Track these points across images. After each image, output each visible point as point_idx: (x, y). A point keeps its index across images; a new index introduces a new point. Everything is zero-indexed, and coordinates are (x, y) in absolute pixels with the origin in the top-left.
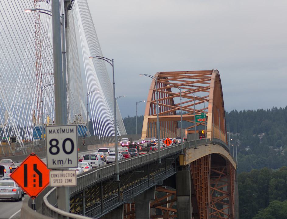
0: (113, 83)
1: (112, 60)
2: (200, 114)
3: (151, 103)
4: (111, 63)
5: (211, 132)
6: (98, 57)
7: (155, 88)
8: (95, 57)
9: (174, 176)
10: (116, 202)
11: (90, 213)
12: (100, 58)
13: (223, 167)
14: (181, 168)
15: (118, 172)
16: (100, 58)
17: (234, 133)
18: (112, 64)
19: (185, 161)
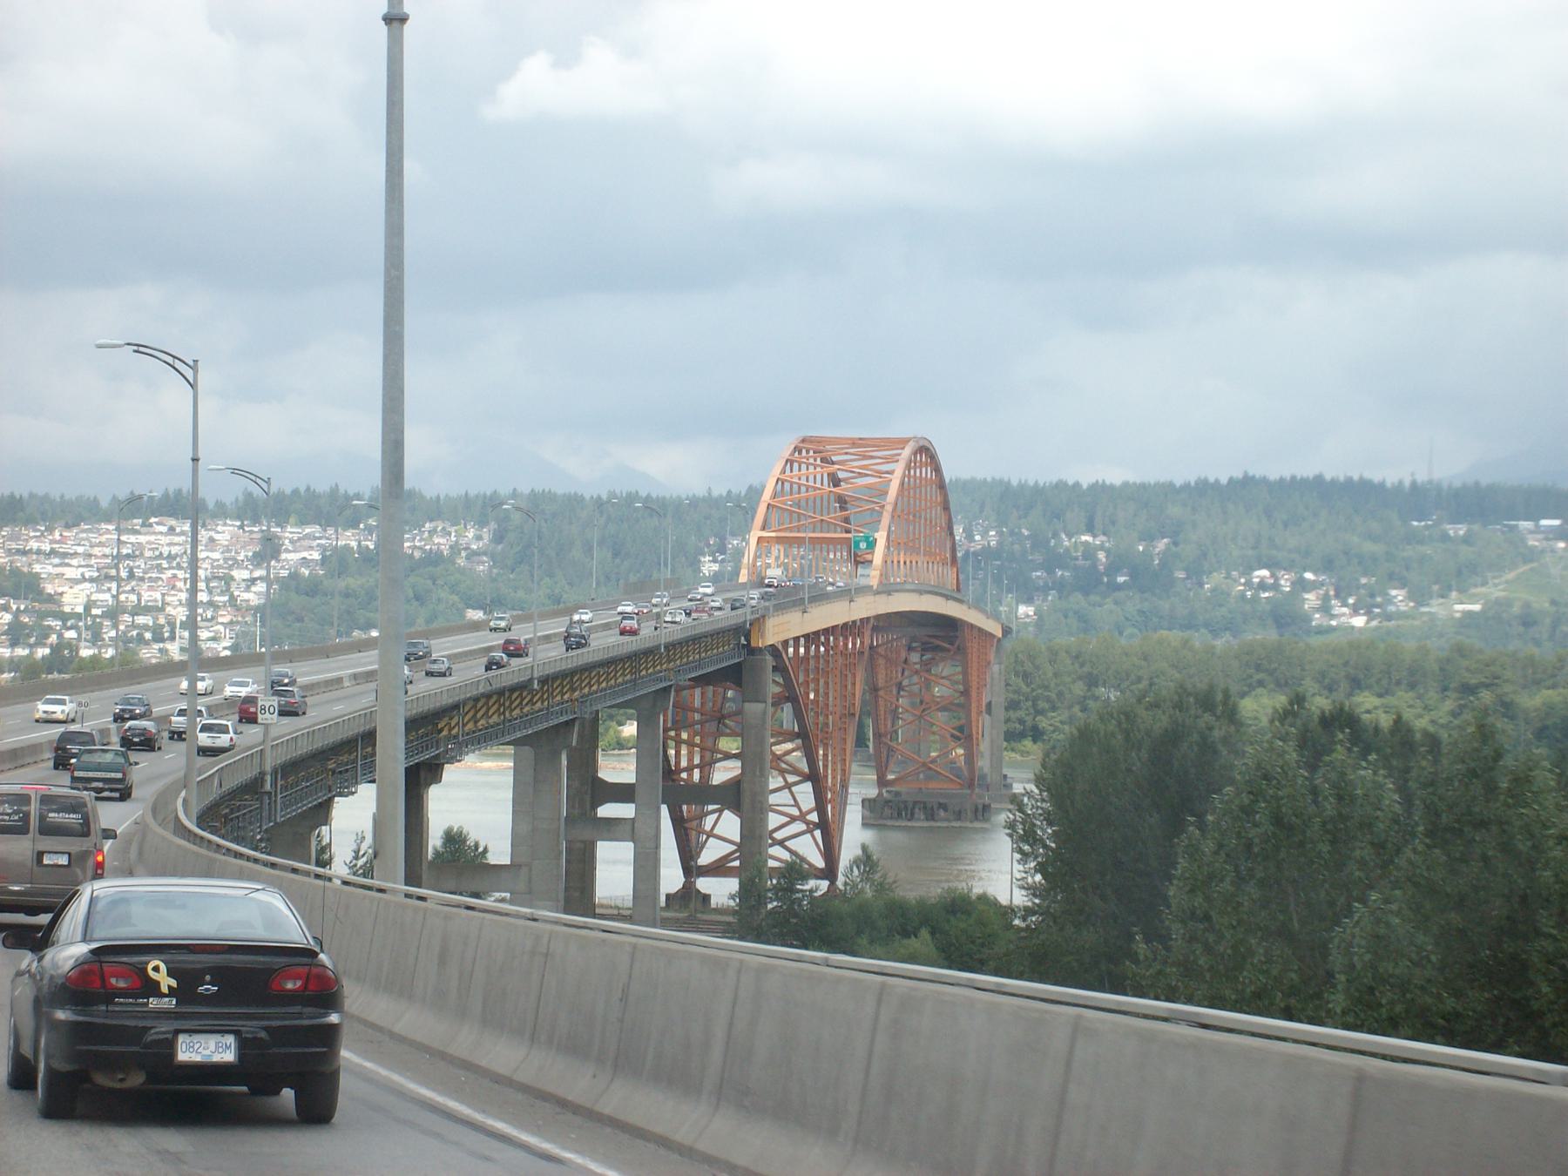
0: (193, 460)
1: (191, 363)
2: (862, 532)
3: (769, 505)
4: (189, 374)
5: (878, 572)
6: (136, 348)
7: (783, 471)
8: (119, 346)
9: (739, 664)
10: (318, 790)
11: (293, 795)
12: (141, 349)
13: (282, 819)
14: (751, 651)
15: (535, 675)
16: (141, 349)
17: (1095, 536)
18: (192, 382)
19: (762, 638)
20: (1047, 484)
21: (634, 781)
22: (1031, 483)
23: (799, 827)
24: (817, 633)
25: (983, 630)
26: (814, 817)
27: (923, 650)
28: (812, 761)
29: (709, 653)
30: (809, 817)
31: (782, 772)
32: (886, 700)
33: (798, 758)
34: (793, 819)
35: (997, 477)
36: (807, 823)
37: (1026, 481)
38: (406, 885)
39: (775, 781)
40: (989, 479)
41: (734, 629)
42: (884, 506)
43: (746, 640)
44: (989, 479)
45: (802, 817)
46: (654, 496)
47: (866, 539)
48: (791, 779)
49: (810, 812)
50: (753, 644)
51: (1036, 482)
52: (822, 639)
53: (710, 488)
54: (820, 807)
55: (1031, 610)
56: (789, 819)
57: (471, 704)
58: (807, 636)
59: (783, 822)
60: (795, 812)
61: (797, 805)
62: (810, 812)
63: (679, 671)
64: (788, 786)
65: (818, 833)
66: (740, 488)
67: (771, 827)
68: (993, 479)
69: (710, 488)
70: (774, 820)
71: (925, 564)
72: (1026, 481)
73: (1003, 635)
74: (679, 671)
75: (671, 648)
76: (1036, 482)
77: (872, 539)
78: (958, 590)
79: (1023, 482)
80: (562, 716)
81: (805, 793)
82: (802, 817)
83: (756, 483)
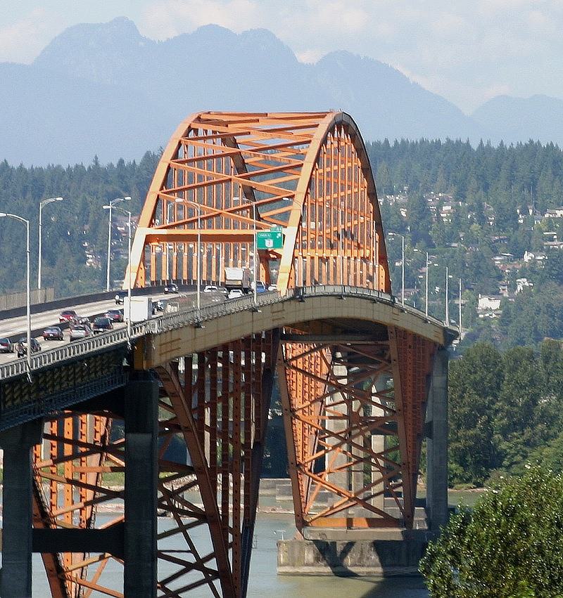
20: (515, 147)
21: (33, 554)
22: (495, 145)
23: (196, 575)
24: (213, 351)
25: (419, 336)
26: (212, 565)
27: (350, 361)
28: (208, 496)
29: (85, 378)
30: (207, 565)
31: (178, 513)
32: (304, 423)
33: (195, 497)
34: (188, 567)
35: (454, 139)
36: (206, 571)
37: (489, 142)
38: (30, 306)
39: (165, 523)
40: (443, 141)
41: (114, 351)
42: (294, 196)
43: (129, 362)
44: (443, 141)
45: (199, 565)
46: (27, 167)
47: (273, 236)
48: (186, 520)
49: (208, 558)
50: (137, 367)
51: (502, 144)
52: (220, 354)
53: (96, 158)
54: (219, 553)
55: (495, 304)
56: (184, 567)
57: (233, 510)
58: (201, 355)
59: (174, 572)
60: (191, 559)
61: (193, 550)
62: (208, 558)
63: (51, 401)
64: (183, 529)
65: (217, 583)
66: (135, 157)
67: (160, 578)
68: (449, 141)
69: (96, 158)
70: (164, 569)
71: (345, 260)
72: (489, 142)
73: (445, 342)
74: (51, 401)
75: (40, 375)
76: (502, 144)
77: (279, 235)
78: (388, 291)
79: (485, 144)
80: (30, 414)
81: (203, 539)
82: (199, 565)
83: (154, 150)
